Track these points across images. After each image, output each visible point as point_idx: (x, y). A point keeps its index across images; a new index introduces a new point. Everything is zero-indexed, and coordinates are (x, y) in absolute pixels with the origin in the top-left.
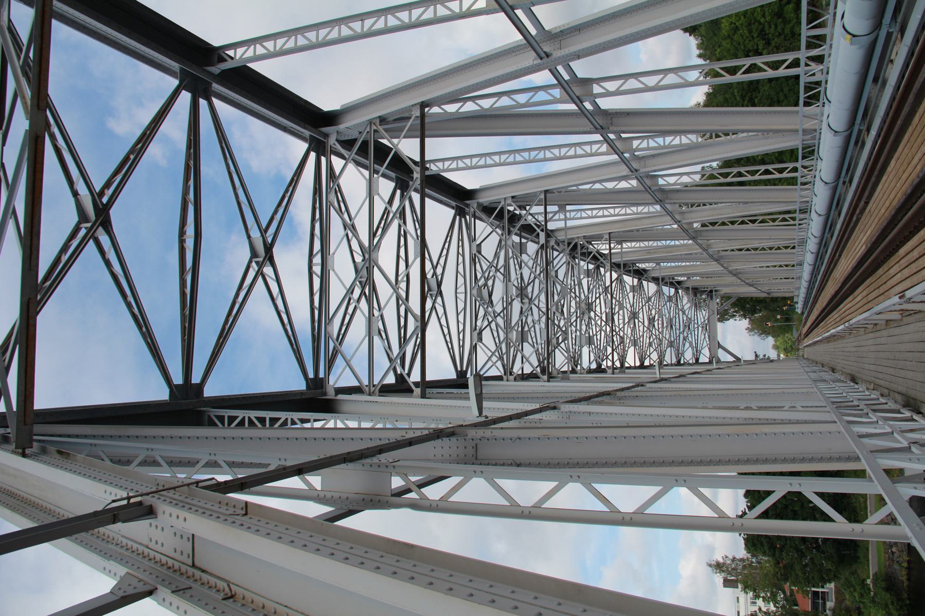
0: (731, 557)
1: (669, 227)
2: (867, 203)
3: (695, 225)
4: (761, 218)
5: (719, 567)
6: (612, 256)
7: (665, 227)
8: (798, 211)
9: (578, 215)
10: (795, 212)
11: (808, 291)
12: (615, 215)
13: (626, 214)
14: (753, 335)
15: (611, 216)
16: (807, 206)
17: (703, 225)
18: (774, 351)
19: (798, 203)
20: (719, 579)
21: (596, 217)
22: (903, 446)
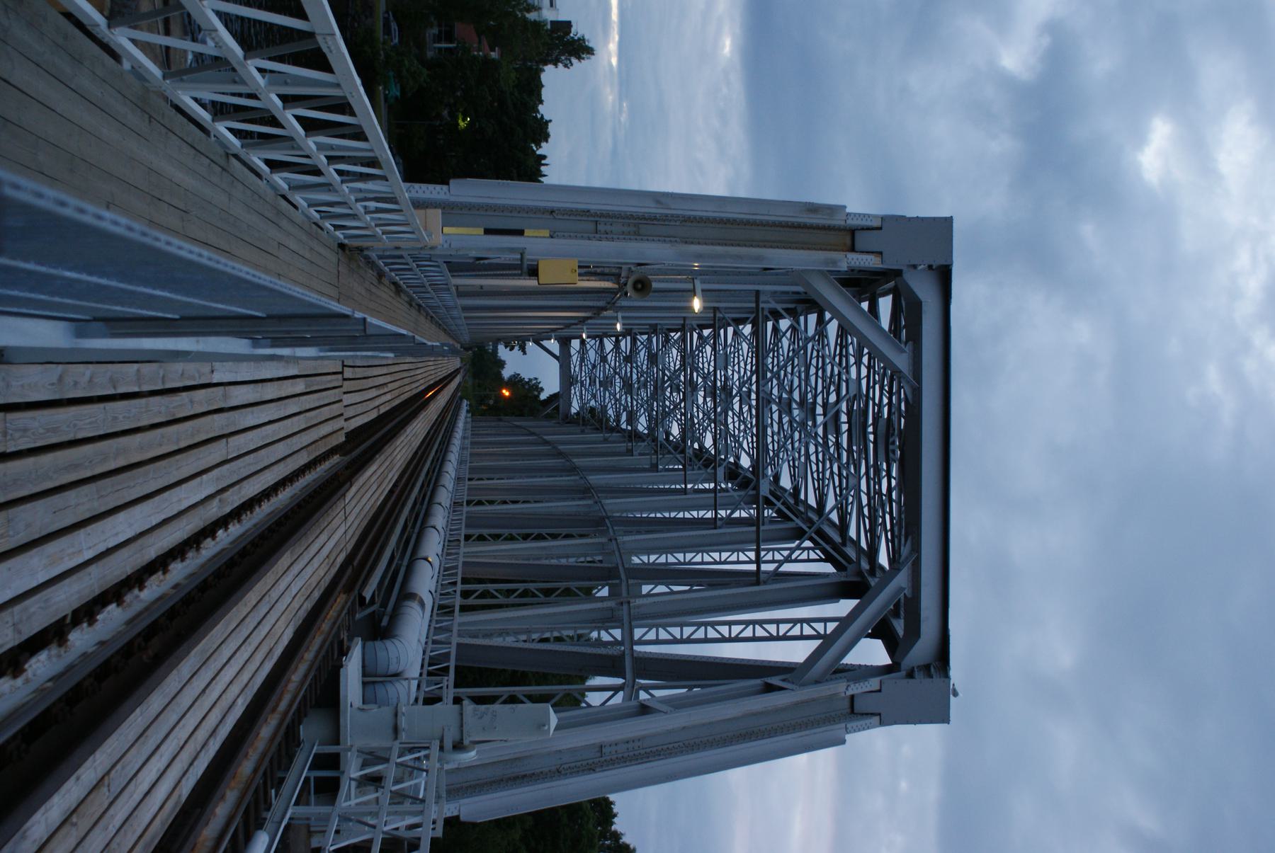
0: (560, 65)
1: (676, 588)
2: (428, 433)
3: (605, 592)
4: (512, 600)
5: (550, 121)
6: (754, 536)
7: (687, 588)
8: (457, 609)
9: (784, 628)
10: (464, 609)
11: (437, 480)
12: (754, 622)
13: (730, 624)
14: (530, 380)
15: (761, 623)
16: (437, 622)
17: (588, 592)
18: (503, 358)
19: (455, 629)
20: (578, 30)
21: (747, 623)
22: (347, 184)
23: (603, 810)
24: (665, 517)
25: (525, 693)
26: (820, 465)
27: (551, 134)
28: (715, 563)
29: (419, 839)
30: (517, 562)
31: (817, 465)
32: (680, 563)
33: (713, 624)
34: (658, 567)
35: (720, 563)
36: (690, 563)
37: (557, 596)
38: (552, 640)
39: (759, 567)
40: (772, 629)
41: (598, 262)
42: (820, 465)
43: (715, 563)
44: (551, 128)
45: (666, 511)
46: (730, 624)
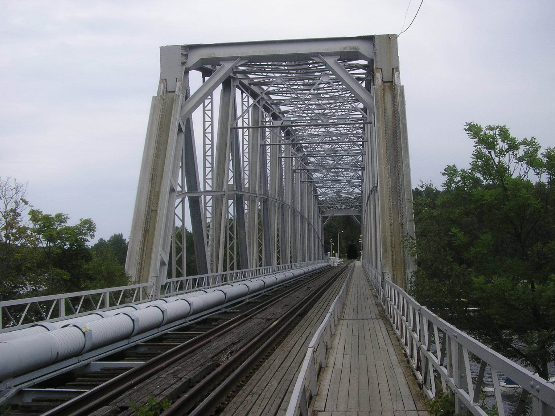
13: (244, 162)
23: (417, 193)
24: (268, 178)
25: (183, 255)
26: (346, 110)
27: (112, 234)
28: (212, 148)
29: (110, 307)
30: (247, 243)
31: (342, 112)
32: (212, 170)
33: (244, 168)
34: (215, 185)
35: (212, 144)
36: (212, 164)
37: (229, 233)
38: (208, 240)
39: (240, 128)
40: (209, 130)
41: (231, 120)
42: (346, 110)
43: (212, 148)
44: (85, 218)
45: (271, 178)
46: (244, 162)
